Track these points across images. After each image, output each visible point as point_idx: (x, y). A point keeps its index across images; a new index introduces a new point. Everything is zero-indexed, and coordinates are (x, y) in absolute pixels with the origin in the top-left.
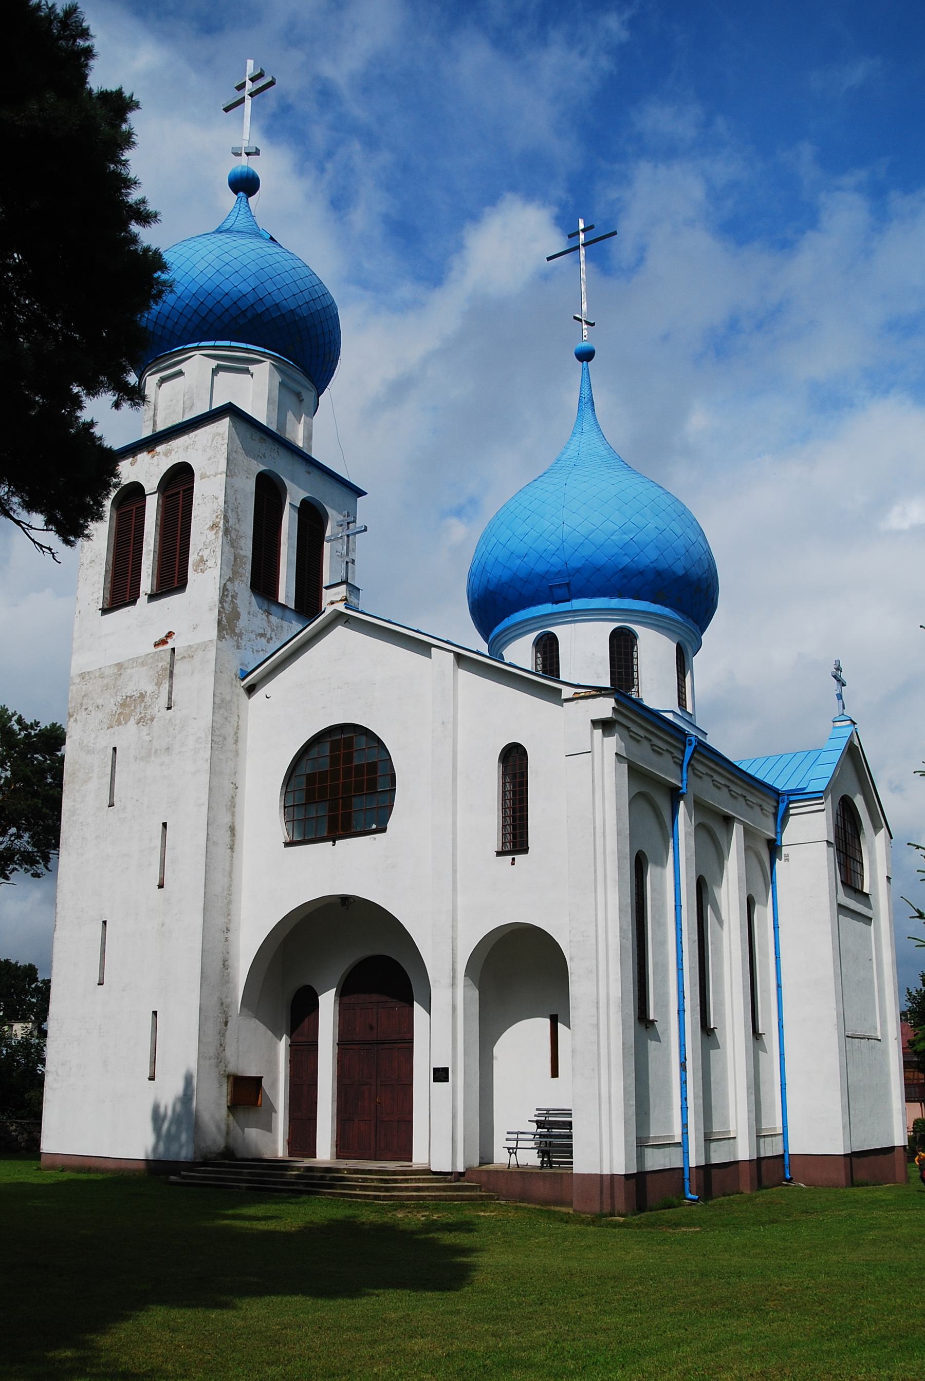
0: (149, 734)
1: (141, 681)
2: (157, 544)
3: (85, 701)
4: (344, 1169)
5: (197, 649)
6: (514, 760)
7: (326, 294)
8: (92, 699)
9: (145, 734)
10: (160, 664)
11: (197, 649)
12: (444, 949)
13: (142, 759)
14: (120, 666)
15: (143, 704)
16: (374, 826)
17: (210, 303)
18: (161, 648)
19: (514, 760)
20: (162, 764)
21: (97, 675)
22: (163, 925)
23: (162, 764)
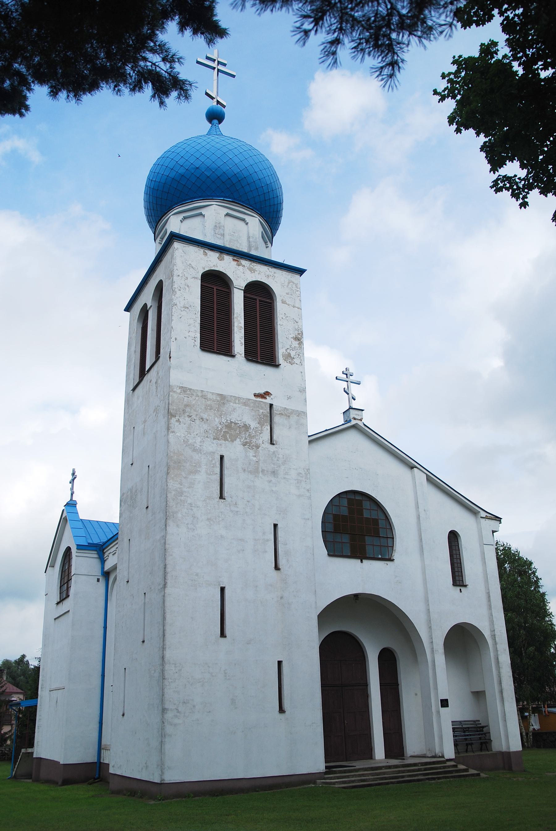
0: (255, 456)
1: (245, 416)
2: (276, 344)
3: (188, 409)
4: (419, 763)
5: (292, 413)
6: (453, 537)
7: (274, 173)
8: (195, 410)
9: (251, 455)
10: (261, 411)
11: (292, 413)
12: (433, 637)
13: (250, 472)
14: (222, 397)
15: (248, 433)
16: (380, 556)
17: (246, 174)
18: (259, 399)
19: (453, 537)
20: (270, 481)
21: (200, 394)
22: (282, 598)
23: (270, 481)
